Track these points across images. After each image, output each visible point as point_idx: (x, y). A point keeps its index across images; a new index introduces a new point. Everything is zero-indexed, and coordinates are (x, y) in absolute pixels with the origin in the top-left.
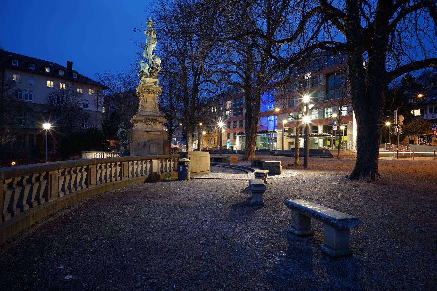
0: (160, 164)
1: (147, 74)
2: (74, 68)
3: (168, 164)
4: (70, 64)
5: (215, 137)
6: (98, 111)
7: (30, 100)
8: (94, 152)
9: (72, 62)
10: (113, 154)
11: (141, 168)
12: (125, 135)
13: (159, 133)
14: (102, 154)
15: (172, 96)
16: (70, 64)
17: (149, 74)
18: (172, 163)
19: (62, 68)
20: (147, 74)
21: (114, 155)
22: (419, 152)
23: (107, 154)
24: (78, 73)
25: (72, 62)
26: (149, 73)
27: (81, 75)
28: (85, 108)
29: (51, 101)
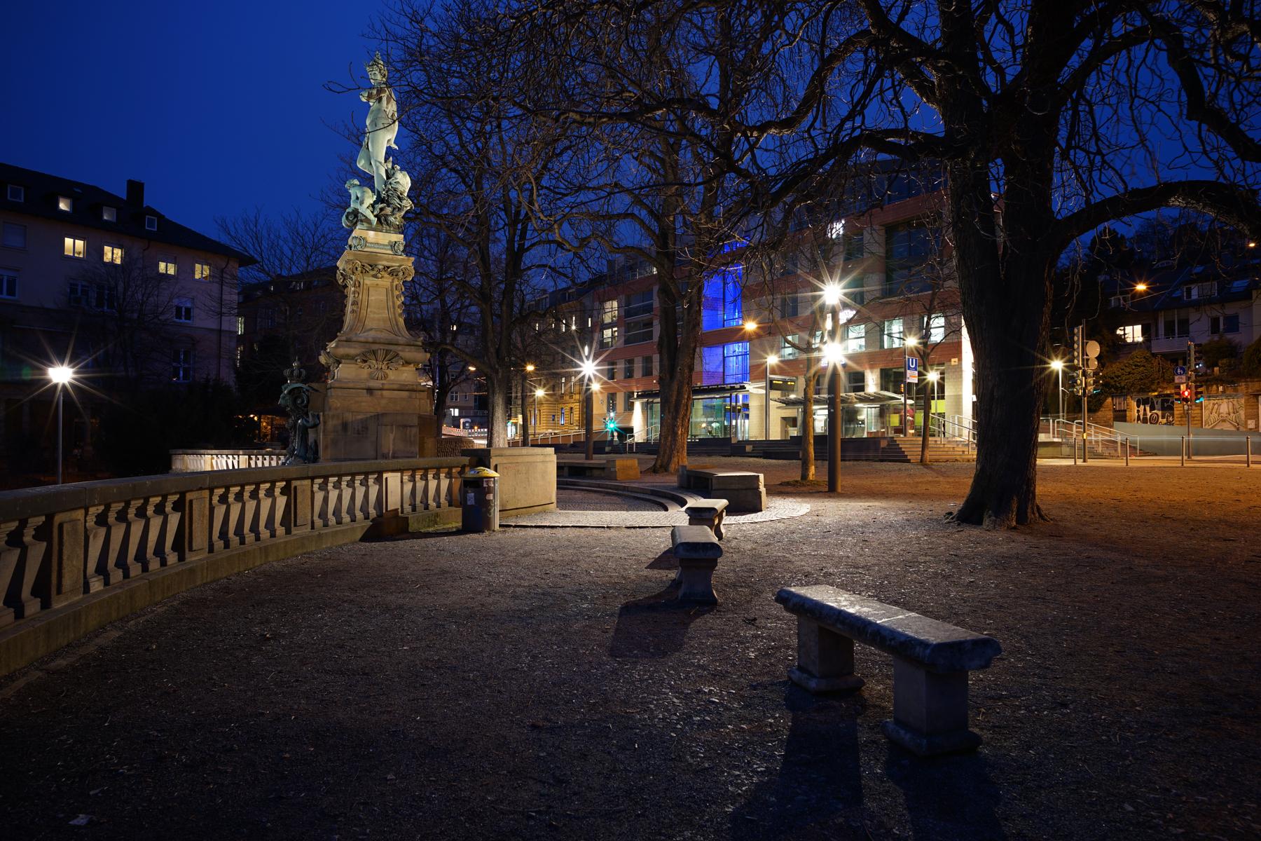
1: (370, 220)
2: (148, 201)
3: (433, 484)
8: (210, 452)
13: (405, 394)
14: (234, 458)
16: (136, 189)
17: (374, 220)
18: (445, 483)
19: (111, 200)
21: (272, 459)
23: (250, 459)
26: (375, 216)
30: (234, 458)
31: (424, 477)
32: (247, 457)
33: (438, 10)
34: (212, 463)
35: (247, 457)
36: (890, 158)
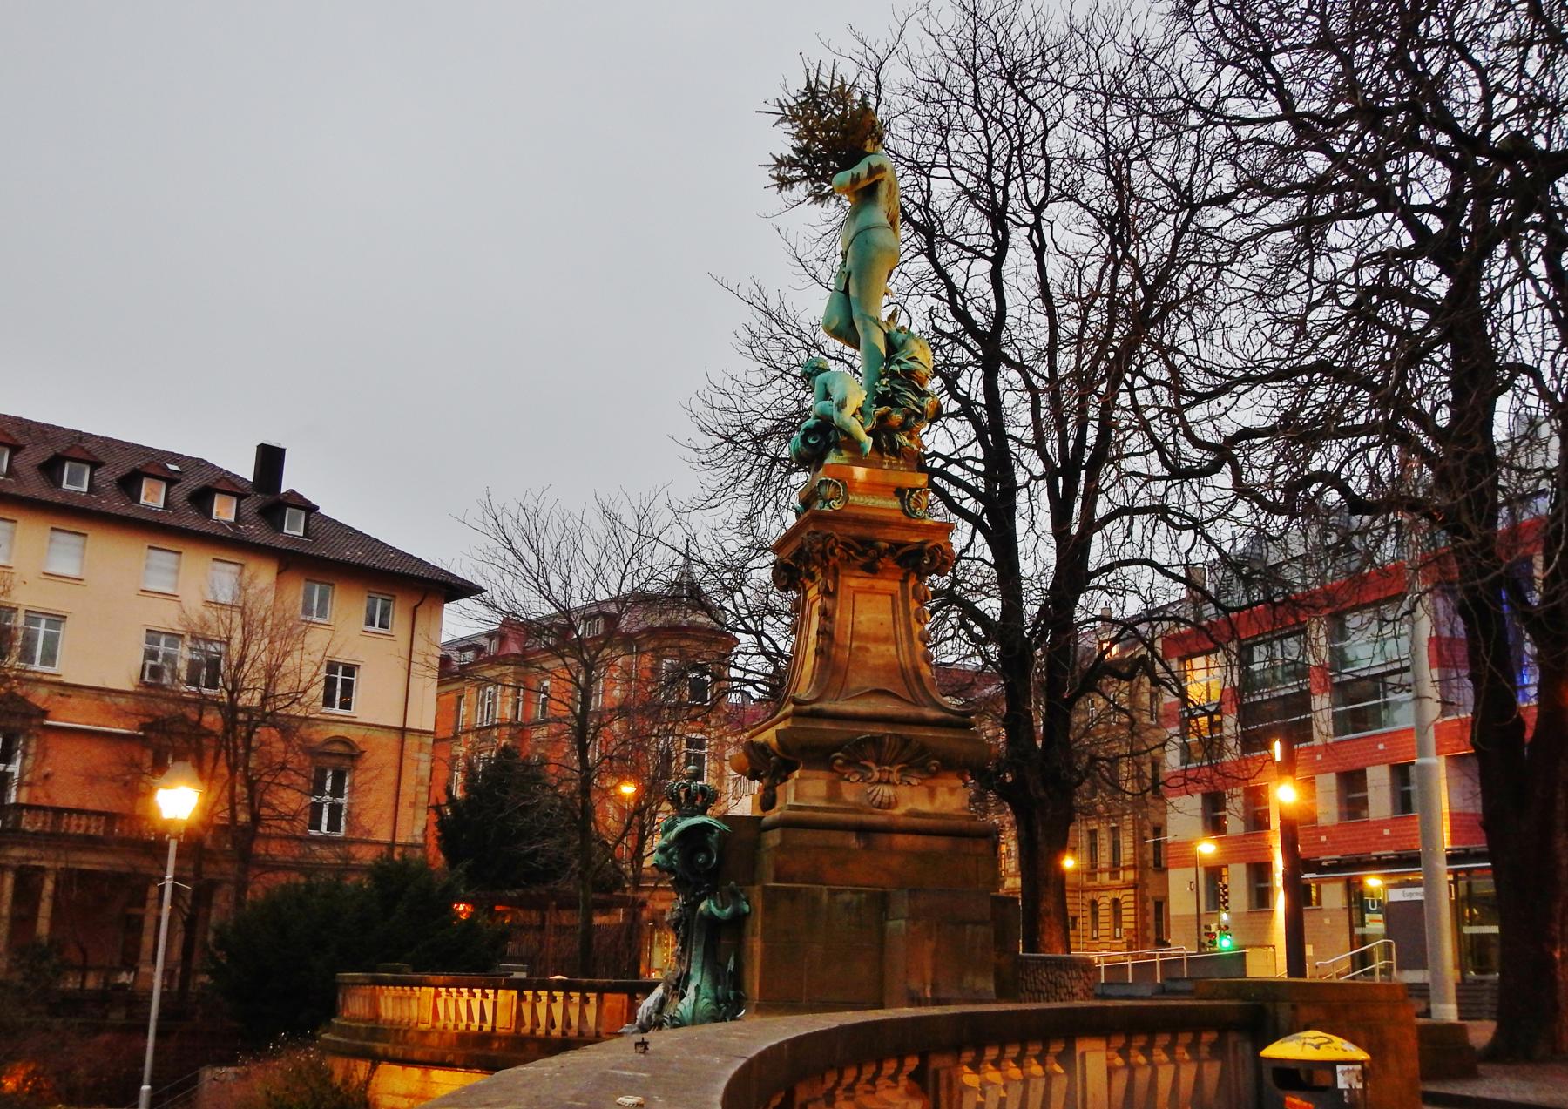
0: (1120, 1081)
1: (858, 442)
2: (290, 481)
3: (1165, 1076)
4: (270, 459)
5: (1118, 895)
6: (408, 726)
7: (44, 663)
8: (432, 978)
9: (283, 450)
10: (559, 995)
11: (1040, 1099)
12: (710, 858)
13: (941, 843)
14: (485, 996)
15: (666, 664)
16: (270, 459)
17: (868, 442)
18: (1188, 1074)
19: (226, 484)
20: (852, 444)
21: (554, 999)
22: (156, 1048)
23: (521, 998)
24: (310, 509)
25: (283, 450)
26: (869, 433)
27: (326, 519)
28: (337, 710)
29: (156, 672)
30: (485, 996)
31: (567, 1023)
32: (514, 993)
33: (918, 43)
34: (519, 1011)
35: (514, 993)
36: (1080, 501)
